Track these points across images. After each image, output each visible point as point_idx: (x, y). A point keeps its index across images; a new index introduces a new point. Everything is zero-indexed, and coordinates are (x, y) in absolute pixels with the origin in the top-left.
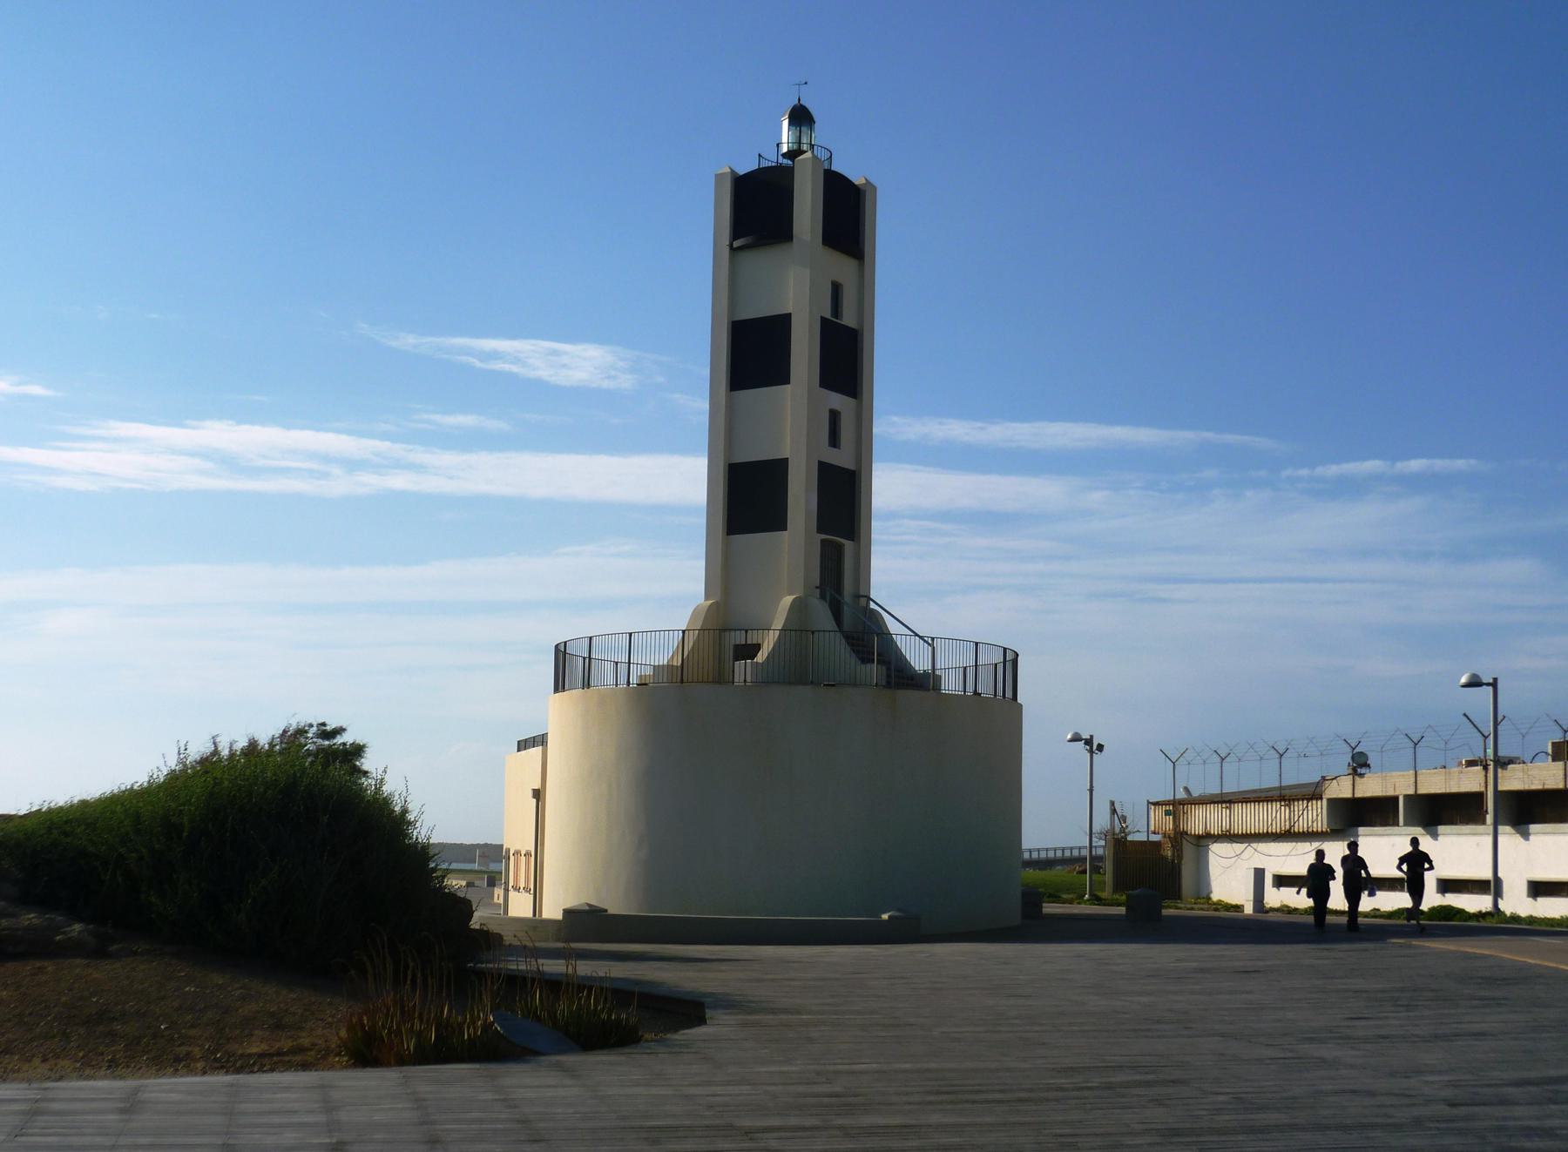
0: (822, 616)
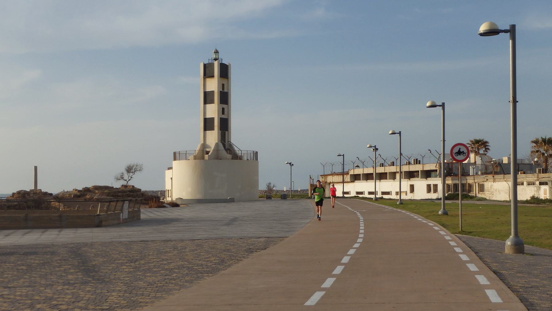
0: (221, 145)
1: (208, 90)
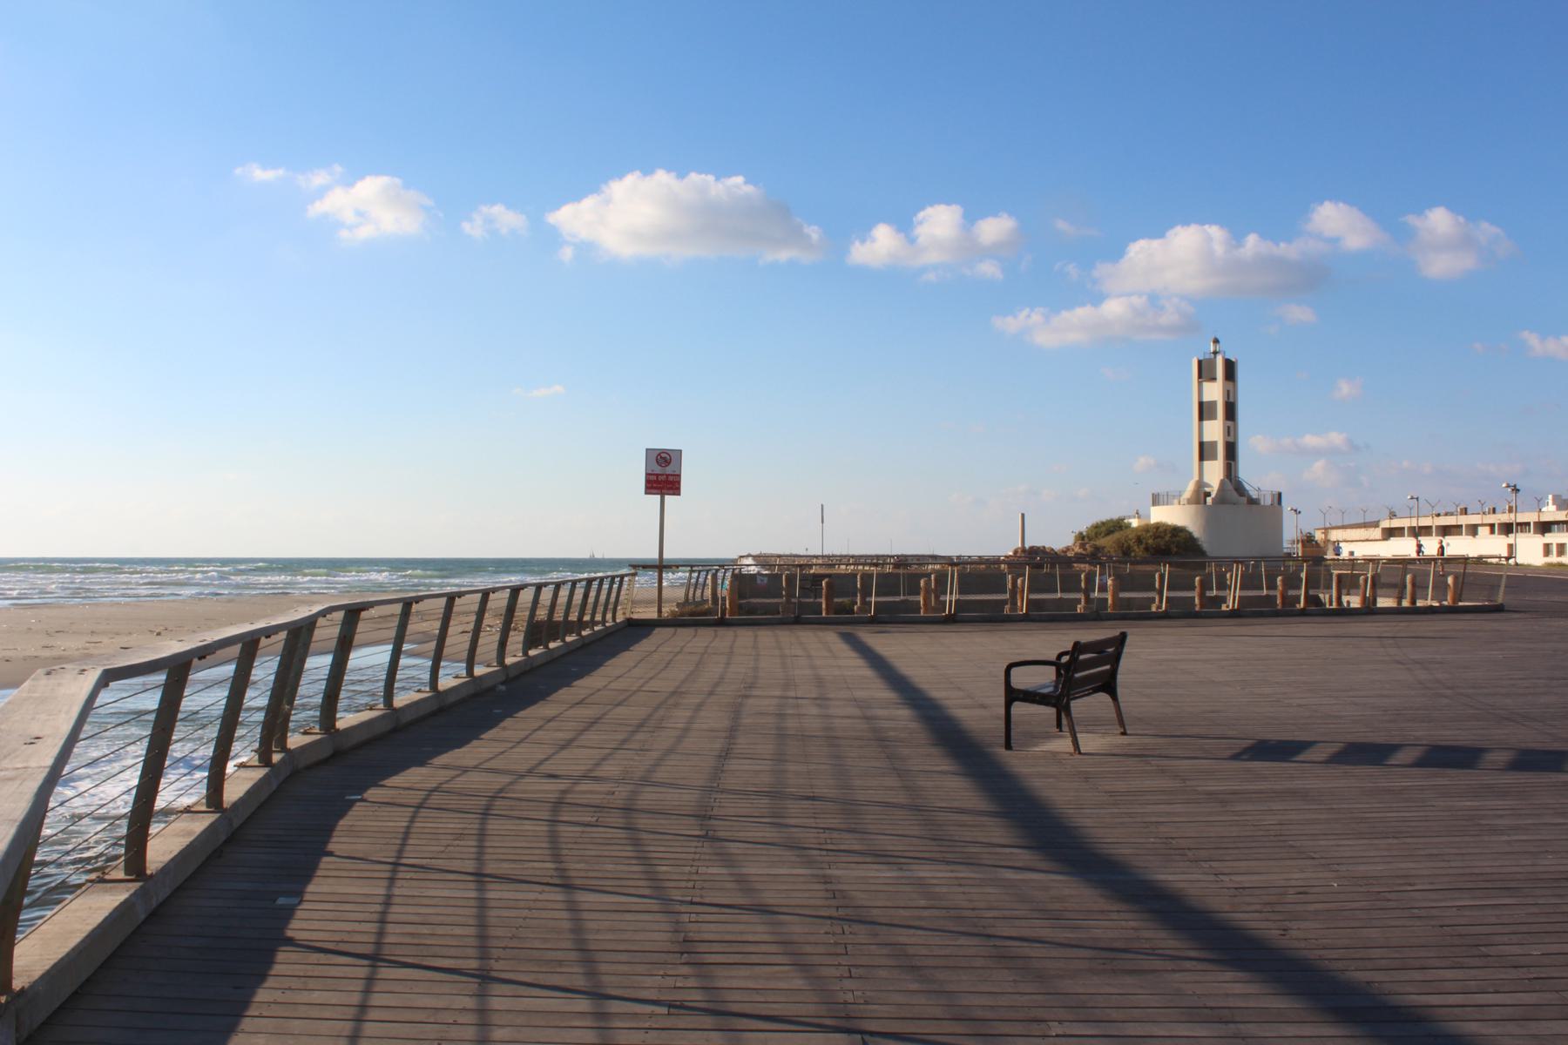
0: (1229, 486)
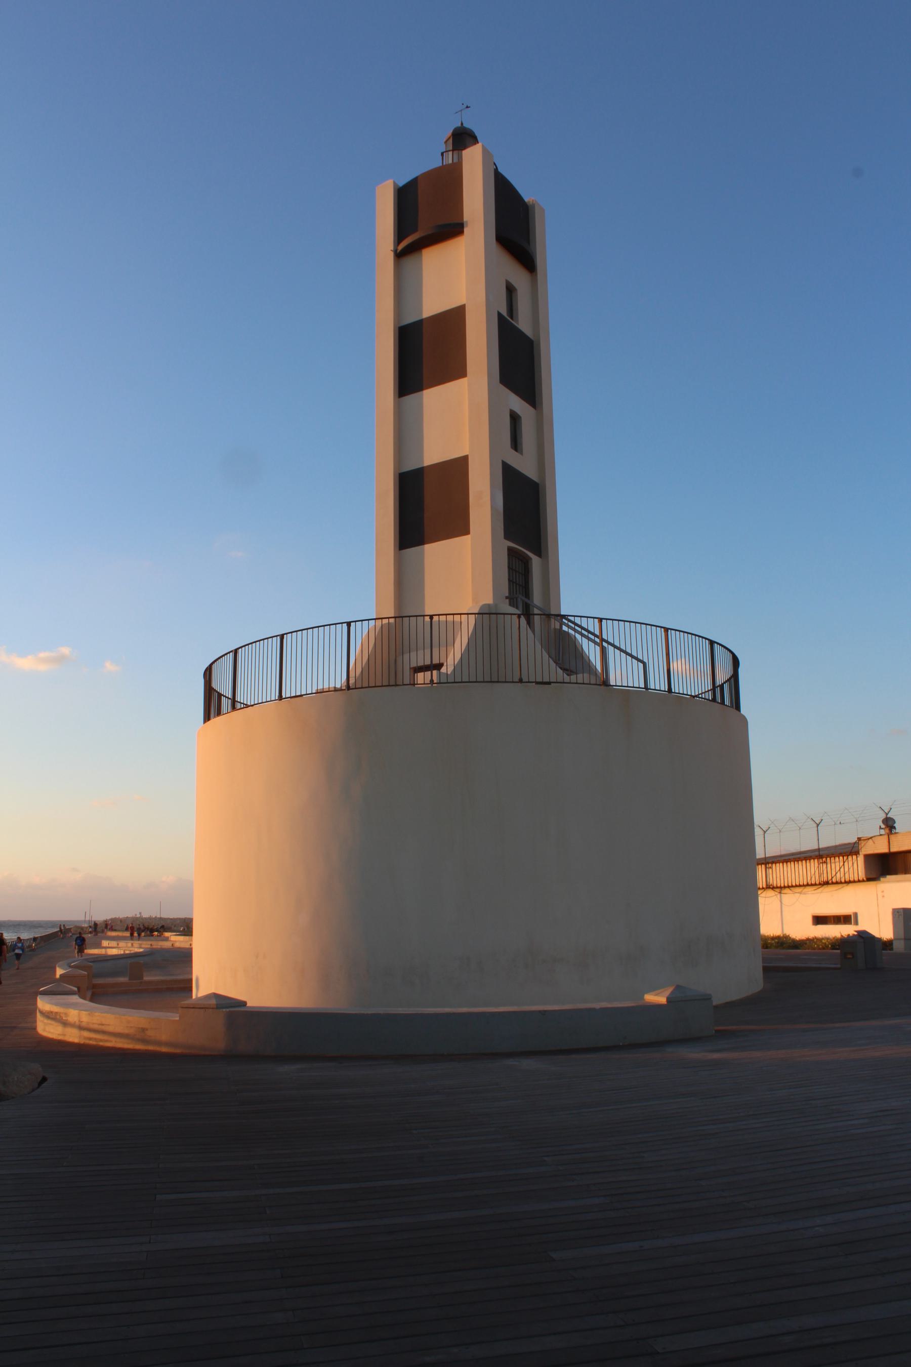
1: (434, 453)
